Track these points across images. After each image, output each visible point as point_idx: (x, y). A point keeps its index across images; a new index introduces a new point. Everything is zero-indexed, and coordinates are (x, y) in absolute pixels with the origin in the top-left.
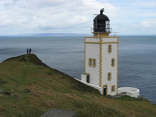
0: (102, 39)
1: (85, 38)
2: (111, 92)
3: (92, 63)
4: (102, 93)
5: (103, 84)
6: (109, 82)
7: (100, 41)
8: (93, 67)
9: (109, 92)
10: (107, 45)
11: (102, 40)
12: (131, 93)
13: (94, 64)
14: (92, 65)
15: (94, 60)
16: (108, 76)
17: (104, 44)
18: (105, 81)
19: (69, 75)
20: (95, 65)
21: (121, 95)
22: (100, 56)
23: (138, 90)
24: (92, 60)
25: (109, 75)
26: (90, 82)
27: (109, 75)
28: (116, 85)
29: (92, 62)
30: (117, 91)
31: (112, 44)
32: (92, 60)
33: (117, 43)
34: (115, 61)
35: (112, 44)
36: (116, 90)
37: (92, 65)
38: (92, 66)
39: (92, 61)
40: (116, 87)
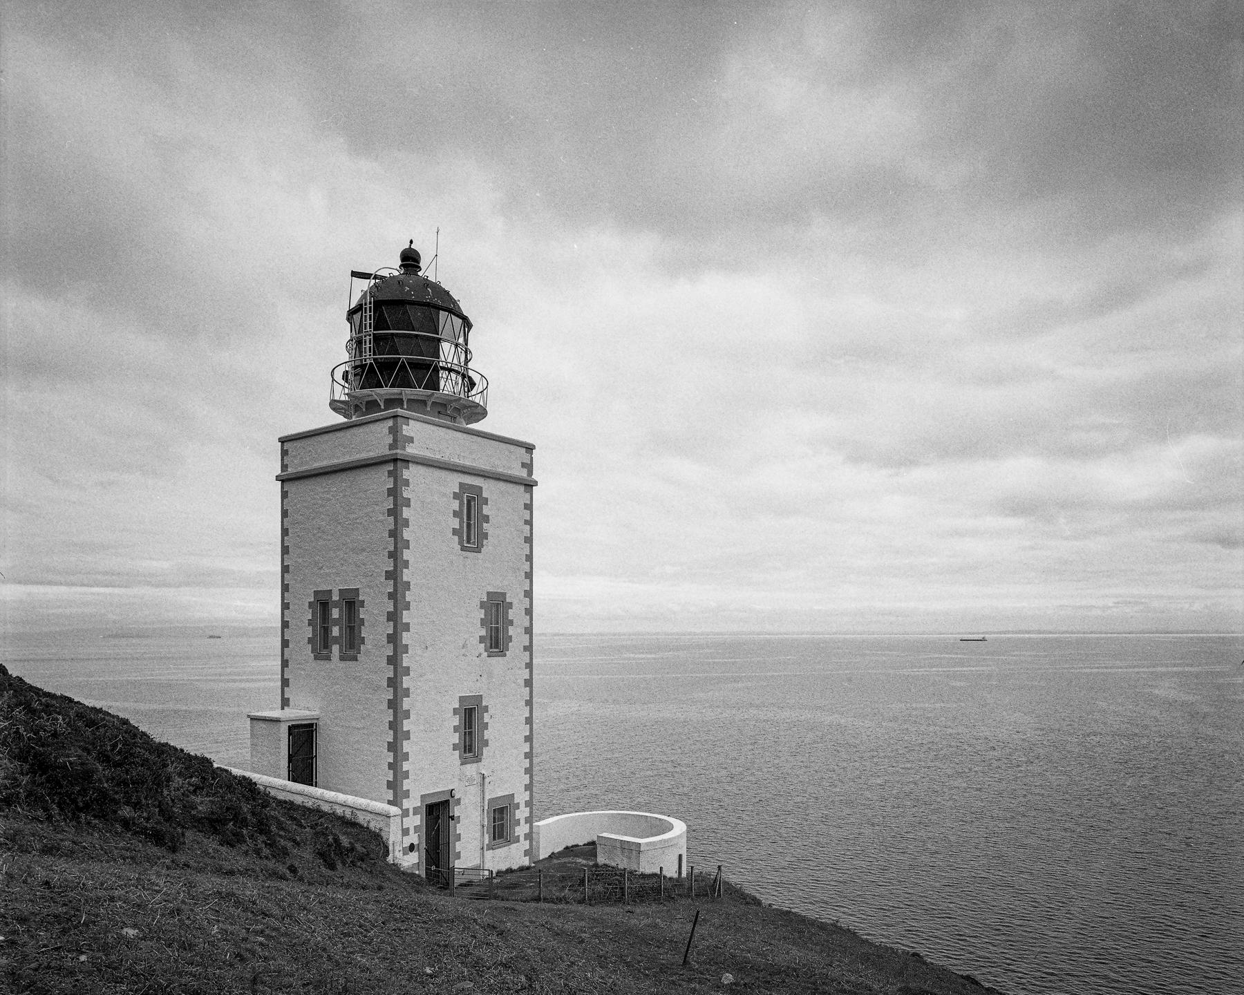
0: (406, 474)
1: (287, 445)
2: (490, 848)
3: (335, 631)
4: (406, 856)
5: (422, 784)
6: (471, 769)
7: (392, 447)
8: (342, 659)
9: (471, 851)
10: (453, 482)
11: (411, 440)
12: (626, 847)
13: (351, 629)
14: (336, 640)
15: (351, 603)
16: (456, 721)
17: (422, 470)
18: (432, 766)
19: (556, 851)
20: (352, 644)
21: (564, 865)
22: (391, 603)
23: (679, 827)
24: (336, 604)
25: (471, 717)
26: (321, 765)
27: (471, 717)
28: (521, 797)
29: (336, 622)
30: (529, 836)
31: (490, 489)
32: (336, 604)
33: (522, 488)
34: (511, 614)
35: (490, 489)
36: (521, 830)
37: (336, 640)
38: (335, 649)
39: (335, 613)
40: (522, 813)
